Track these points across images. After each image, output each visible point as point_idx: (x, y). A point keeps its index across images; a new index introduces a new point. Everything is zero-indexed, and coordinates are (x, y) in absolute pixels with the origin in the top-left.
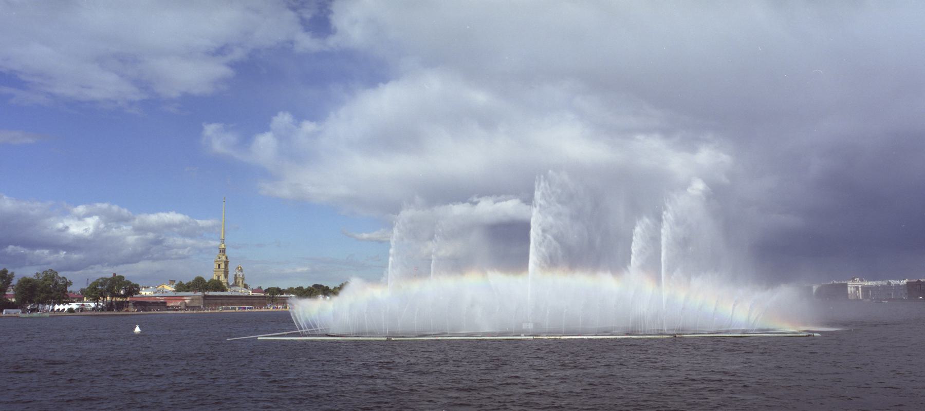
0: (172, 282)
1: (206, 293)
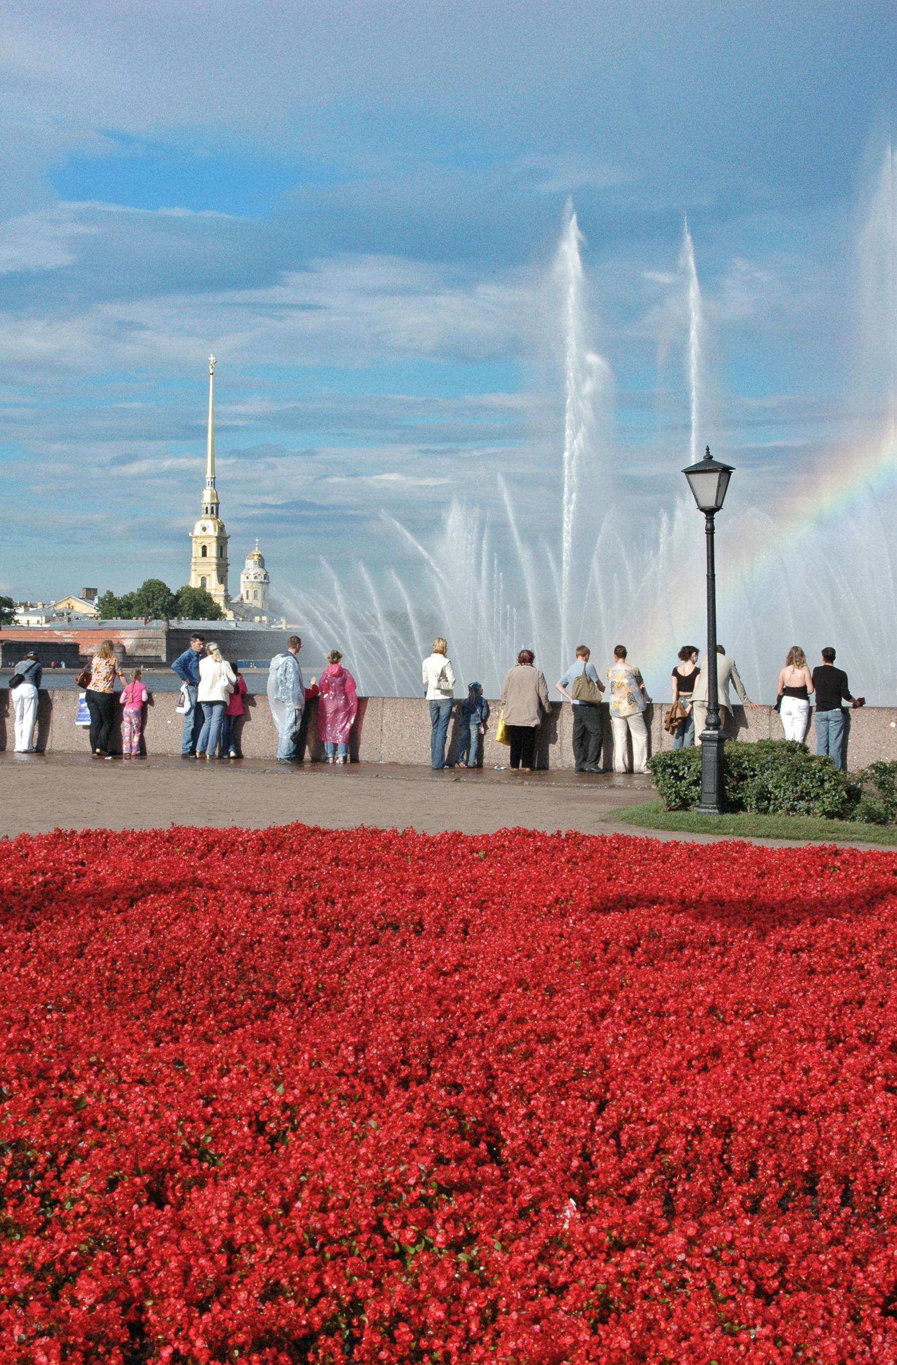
0: (90, 593)
1: (174, 624)
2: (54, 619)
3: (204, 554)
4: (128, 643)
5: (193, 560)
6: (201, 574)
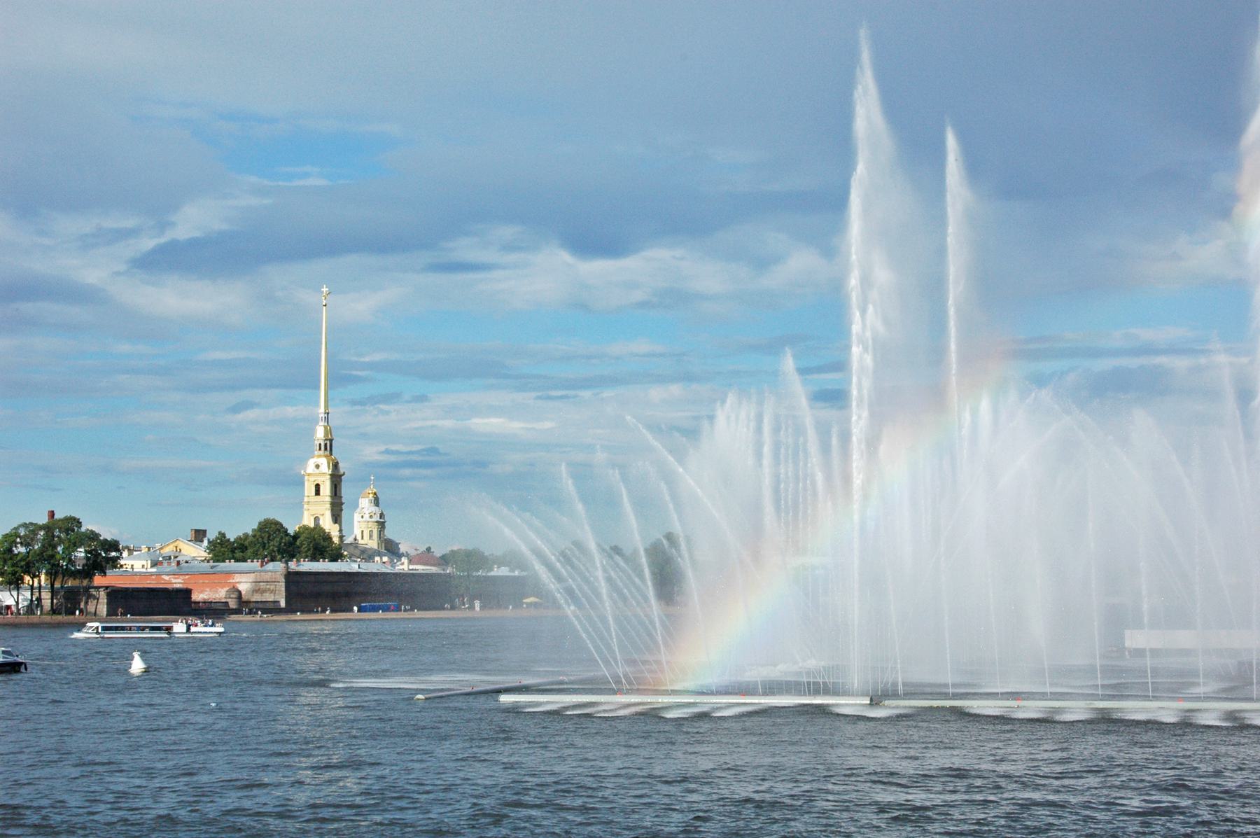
0: (199, 535)
1: (293, 566)
2: (161, 563)
3: (318, 493)
4: (244, 587)
5: (306, 499)
6: (313, 513)
